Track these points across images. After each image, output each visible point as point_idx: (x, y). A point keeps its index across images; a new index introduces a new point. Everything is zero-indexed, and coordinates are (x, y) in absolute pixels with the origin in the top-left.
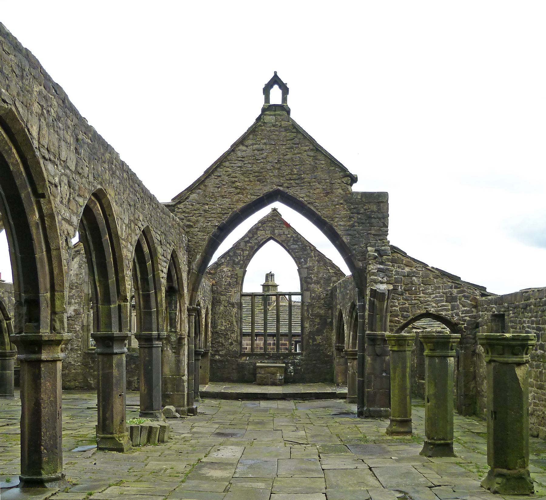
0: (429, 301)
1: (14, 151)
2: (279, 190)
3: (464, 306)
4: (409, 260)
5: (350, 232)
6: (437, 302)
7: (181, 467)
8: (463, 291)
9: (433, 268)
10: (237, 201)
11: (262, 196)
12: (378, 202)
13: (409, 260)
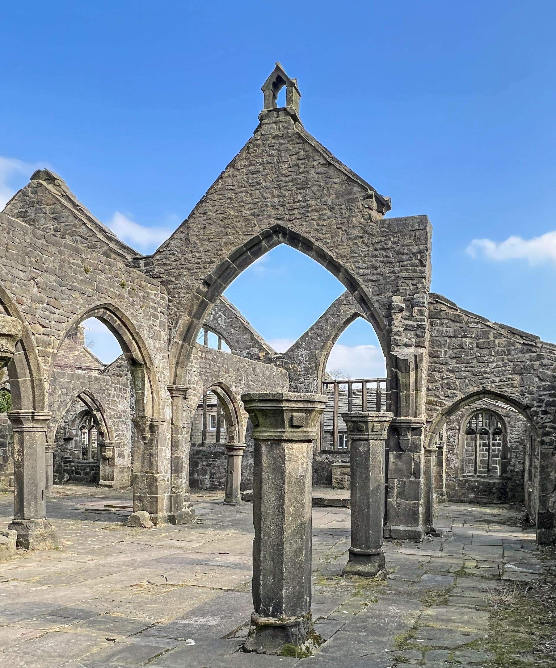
2: (278, 225)
6: (498, 374)
8: (540, 357)
9: (496, 324)
13: (458, 313)
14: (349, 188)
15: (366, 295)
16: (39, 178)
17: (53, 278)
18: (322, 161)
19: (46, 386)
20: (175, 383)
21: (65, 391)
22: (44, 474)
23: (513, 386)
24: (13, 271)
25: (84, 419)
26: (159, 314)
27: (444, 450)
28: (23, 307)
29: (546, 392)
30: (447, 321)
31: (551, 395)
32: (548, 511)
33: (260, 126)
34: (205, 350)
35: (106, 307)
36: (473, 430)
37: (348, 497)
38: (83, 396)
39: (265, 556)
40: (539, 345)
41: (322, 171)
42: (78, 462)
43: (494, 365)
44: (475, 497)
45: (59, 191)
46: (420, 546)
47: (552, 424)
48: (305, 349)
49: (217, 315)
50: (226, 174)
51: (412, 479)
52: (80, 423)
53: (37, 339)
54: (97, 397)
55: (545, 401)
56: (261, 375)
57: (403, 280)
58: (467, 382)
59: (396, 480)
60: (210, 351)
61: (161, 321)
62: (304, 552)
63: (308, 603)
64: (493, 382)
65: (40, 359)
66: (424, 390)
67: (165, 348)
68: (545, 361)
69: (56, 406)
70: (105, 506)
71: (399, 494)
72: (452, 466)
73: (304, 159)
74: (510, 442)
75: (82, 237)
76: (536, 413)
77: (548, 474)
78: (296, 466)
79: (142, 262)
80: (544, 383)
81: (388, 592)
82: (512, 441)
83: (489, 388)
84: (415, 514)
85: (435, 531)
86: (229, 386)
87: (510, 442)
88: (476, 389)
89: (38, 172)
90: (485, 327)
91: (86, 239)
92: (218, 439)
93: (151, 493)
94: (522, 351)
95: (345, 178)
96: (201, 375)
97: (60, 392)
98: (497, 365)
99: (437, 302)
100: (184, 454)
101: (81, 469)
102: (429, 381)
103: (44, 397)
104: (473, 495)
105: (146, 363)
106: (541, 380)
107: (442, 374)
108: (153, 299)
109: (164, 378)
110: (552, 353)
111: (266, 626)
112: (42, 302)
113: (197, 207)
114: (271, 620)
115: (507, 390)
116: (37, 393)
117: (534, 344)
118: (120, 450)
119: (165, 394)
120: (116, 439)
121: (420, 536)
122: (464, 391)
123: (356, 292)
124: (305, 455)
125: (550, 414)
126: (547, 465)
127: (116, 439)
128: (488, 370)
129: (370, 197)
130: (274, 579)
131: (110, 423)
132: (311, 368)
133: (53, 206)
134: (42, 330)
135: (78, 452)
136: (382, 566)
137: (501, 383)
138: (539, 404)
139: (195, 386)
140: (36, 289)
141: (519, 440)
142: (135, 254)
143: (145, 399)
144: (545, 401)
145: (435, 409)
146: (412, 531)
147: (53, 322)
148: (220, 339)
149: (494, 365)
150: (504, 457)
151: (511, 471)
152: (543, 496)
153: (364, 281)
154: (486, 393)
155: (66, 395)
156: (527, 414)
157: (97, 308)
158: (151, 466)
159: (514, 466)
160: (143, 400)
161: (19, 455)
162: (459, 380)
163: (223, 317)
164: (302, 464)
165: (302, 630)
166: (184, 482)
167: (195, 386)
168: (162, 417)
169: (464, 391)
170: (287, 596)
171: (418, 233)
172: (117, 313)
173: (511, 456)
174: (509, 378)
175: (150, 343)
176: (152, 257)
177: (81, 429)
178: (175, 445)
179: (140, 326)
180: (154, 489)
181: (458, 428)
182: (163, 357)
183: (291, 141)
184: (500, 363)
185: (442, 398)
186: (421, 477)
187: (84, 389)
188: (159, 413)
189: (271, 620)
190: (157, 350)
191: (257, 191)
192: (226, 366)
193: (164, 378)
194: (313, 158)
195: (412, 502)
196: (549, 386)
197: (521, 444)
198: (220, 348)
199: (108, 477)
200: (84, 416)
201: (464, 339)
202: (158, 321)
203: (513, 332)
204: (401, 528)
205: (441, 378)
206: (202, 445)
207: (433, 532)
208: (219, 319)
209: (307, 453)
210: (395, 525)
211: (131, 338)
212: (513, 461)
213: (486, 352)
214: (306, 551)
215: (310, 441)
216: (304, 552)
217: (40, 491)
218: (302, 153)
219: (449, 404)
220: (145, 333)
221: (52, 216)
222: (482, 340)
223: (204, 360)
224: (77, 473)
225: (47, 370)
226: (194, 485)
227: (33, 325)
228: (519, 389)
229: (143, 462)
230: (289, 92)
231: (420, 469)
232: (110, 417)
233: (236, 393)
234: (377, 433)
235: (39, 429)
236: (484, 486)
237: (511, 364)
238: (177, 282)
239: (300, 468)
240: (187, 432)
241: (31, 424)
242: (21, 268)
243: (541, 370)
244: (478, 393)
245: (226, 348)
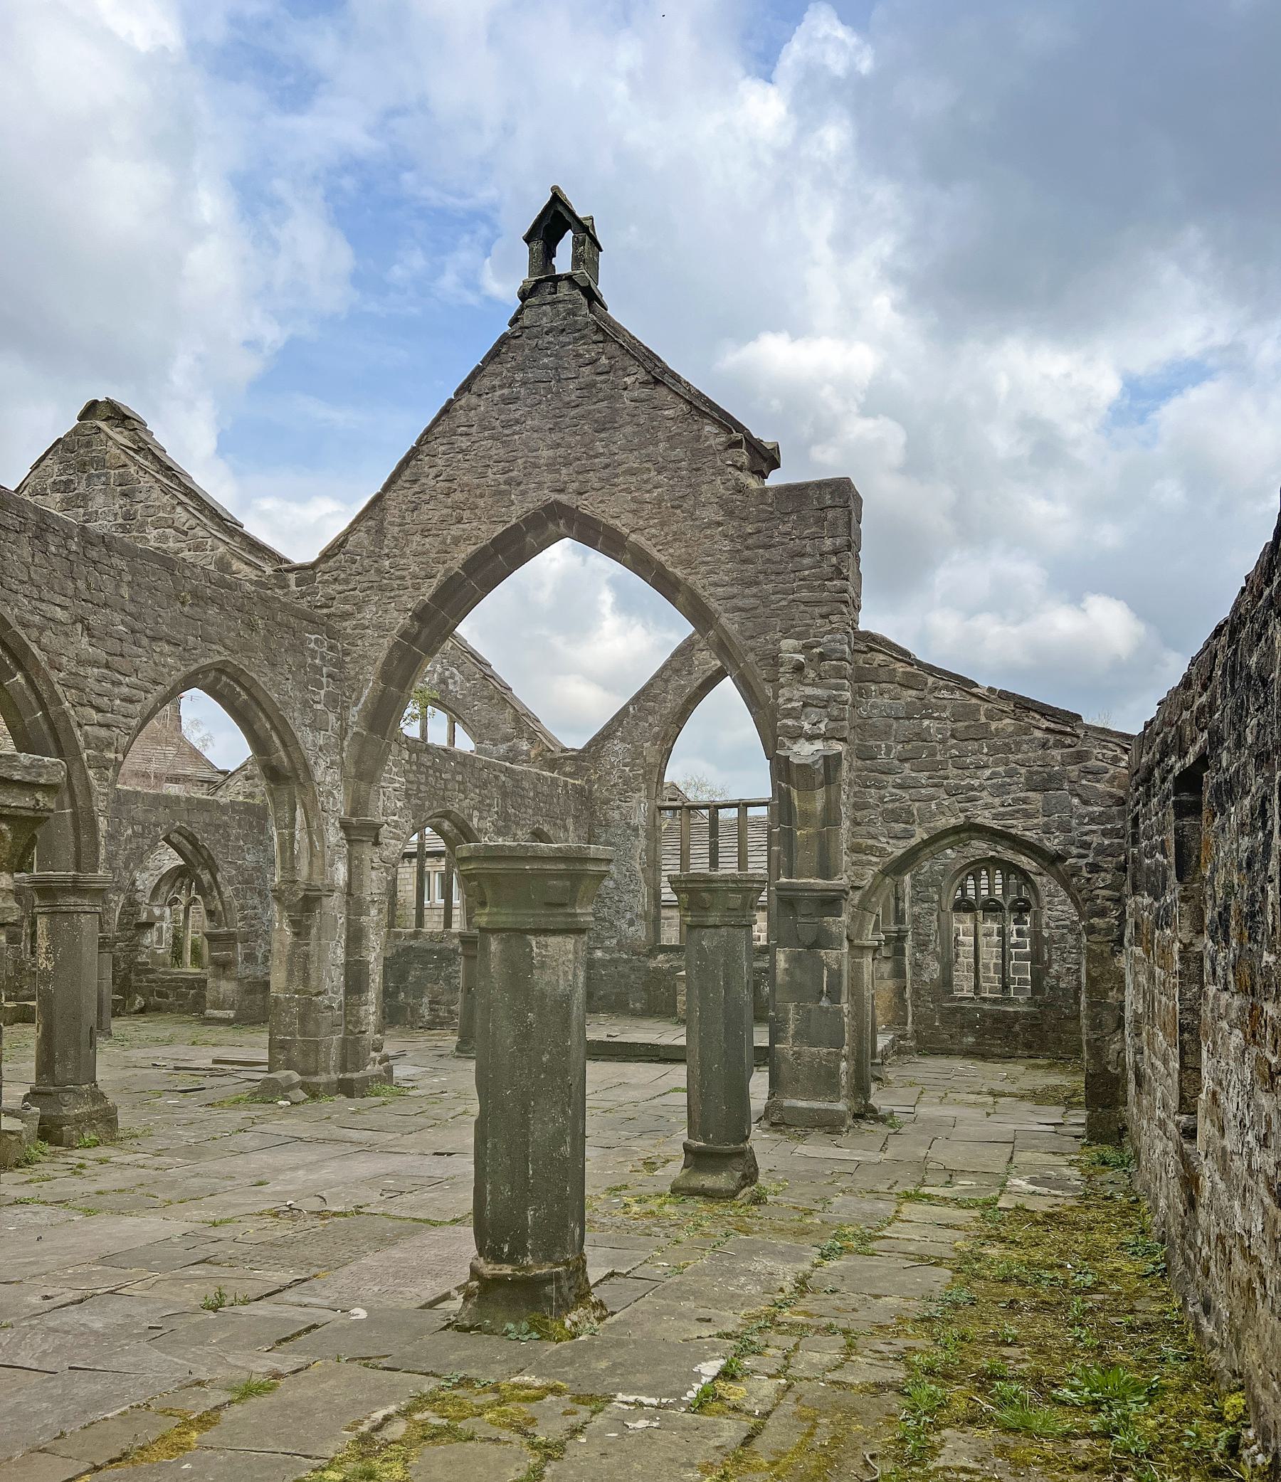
0: (973, 788)
1: (275, 738)
2: (557, 503)
3: (1086, 803)
4: (914, 670)
5: (739, 602)
6: (1000, 790)
7: (212, 611)
8: (1081, 757)
9: (991, 690)
10: (456, 541)
11: (514, 521)
12: (836, 502)
13: (914, 670)
14: (695, 427)
15: (729, 638)
16: (95, 417)
17: (117, 617)
18: (642, 375)
19: (103, 823)
20: (353, 814)
21: (138, 828)
22: (95, 996)
23: (1028, 815)
24: (44, 606)
25: (178, 884)
26: (324, 680)
27: (908, 945)
28: (62, 675)
29: (1094, 828)
30: (891, 686)
31: (1105, 834)
32: (1106, 1069)
33: (520, 311)
34: (420, 747)
35: (221, 669)
36: (969, 902)
37: (682, 1041)
38: (175, 838)
39: (495, 1146)
40: (1081, 732)
41: (643, 396)
42: (163, 973)
43: (988, 772)
44: (978, 1044)
45: (134, 442)
46: (840, 1140)
47: (1110, 893)
48: (623, 740)
49: (447, 673)
50: (457, 405)
51: (825, 1003)
52: (168, 892)
53: (86, 735)
54: (204, 839)
55: (1094, 845)
56: (532, 794)
57: (802, 607)
58: (933, 807)
59: (791, 1006)
60: (429, 749)
61: (328, 694)
62: (568, 1139)
63: (577, 1237)
64: (987, 806)
65: (91, 773)
66: (846, 824)
67: (336, 745)
68: (1092, 763)
69: (120, 863)
70: (215, 1062)
71: (798, 1035)
72: (926, 977)
73: (607, 373)
74: (1048, 926)
75: (176, 529)
76: (1076, 872)
77: (1105, 994)
78: (554, 978)
79: (292, 577)
80: (1090, 809)
81: (756, 1229)
82: (1052, 925)
83: (979, 820)
84: (833, 1074)
85: (874, 1111)
86: (465, 817)
87: (1048, 926)
88: (953, 821)
89: (94, 404)
90: (968, 697)
91: (186, 534)
92: (448, 923)
93: (304, 1034)
94: (1044, 745)
95: (685, 407)
96: (408, 796)
97: (130, 832)
98: (993, 773)
99: (872, 649)
100: (374, 955)
101: (168, 987)
102: (857, 807)
103: (97, 845)
104: (971, 1039)
105: (298, 776)
106: (1086, 803)
107: (882, 792)
108: (313, 650)
109: (334, 804)
110: (1104, 747)
111: (498, 1281)
112: (95, 663)
113: (436, 422)
114: (507, 1270)
115: (1014, 822)
116: (84, 838)
117: (1069, 729)
118: (249, 947)
119: (334, 836)
120: (240, 924)
121: (843, 1123)
122: (927, 825)
123: (711, 633)
124: (571, 956)
125: (1105, 871)
126: (1102, 975)
127: (240, 924)
128: (976, 783)
129: (737, 444)
130: (512, 1190)
131: (228, 891)
132: (636, 777)
133: (122, 470)
134: (96, 717)
135: (163, 950)
136: (750, 1177)
137: (1002, 809)
138: (1081, 851)
139: (396, 818)
140: (85, 639)
141: (1068, 923)
142: (281, 560)
143: (296, 845)
144: (1094, 845)
145: (870, 863)
146: (826, 1110)
147: (118, 702)
148: (452, 723)
149: (988, 772)
150: (1035, 957)
151: (1052, 988)
152: (1096, 1040)
153: (726, 611)
154: (972, 829)
155: (142, 835)
156: (1059, 872)
157: (204, 670)
158: (306, 979)
159: (1058, 978)
160: (292, 848)
161: (48, 959)
162: (917, 804)
163: (459, 677)
164: (565, 973)
165: (565, 1290)
166: (371, 1011)
167: (396, 818)
168: (327, 882)
169: (927, 825)
170: (535, 1223)
171: (830, 514)
172: (242, 680)
173: (1050, 956)
174: (1019, 799)
175: (307, 738)
176: (313, 566)
177: (170, 905)
178: (355, 937)
179: (286, 703)
180: (311, 1026)
181: (936, 897)
182: (333, 763)
183: (582, 337)
184: (1001, 769)
185: (884, 840)
186: (844, 999)
187: (178, 824)
188: (323, 873)
189: (507, 1270)
190: (321, 750)
191: (516, 437)
192: (459, 778)
193: (334, 804)
194: (624, 369)
195: (825, 1050)
196: (1102, 813)
197: (1071, 931)
198: (452, 740)
199: (224, 1001)
200: (175, 881)
201: (926, 722)
202: (322, 692)
203: (1024, 706)
204: (802, 1104)
205: (881, 799)
206: (416, 935)
207: (865, 1113)
208: (450, 681)
209: (576, 952)
210: (792, 1097)
211: (268, 726)
212: (1056, 966)
213: (972, 746)
214: (573, 1139)
215: (580, 931)
216: (568, 1139)
217: (85, 1030)
218: (604, 360)
219: (897, 849)
220: (295, 718)
221: (119, 489)
222: (962, 724)
223: (414, 768)
224: (160, 994)
225: (105, 794)
226: (393, 1016)
227: (79, 708)
228: (1041, 820)
229: (290, 973)
230: (577, 243)
231: (840, 983)
232: (230, 881)
233: (479, 830)
234: (735, 913)
235: (87, 909)
236: (996, 1020)
237: (1023, 770)
238: (359, 616)
239: (561, 982)
240: (380, 911)
241: (72, 900)
242: (59, 599)
243: (1084, 782)
244: (956, 830)
245: (465, 743)
